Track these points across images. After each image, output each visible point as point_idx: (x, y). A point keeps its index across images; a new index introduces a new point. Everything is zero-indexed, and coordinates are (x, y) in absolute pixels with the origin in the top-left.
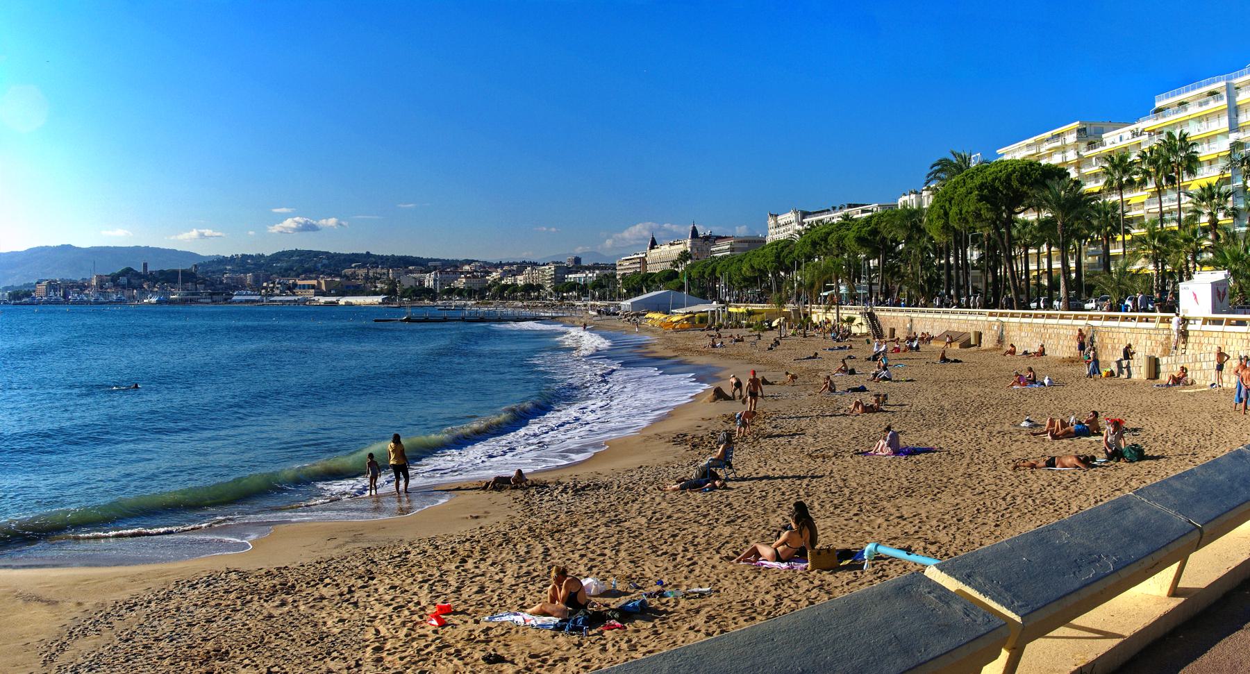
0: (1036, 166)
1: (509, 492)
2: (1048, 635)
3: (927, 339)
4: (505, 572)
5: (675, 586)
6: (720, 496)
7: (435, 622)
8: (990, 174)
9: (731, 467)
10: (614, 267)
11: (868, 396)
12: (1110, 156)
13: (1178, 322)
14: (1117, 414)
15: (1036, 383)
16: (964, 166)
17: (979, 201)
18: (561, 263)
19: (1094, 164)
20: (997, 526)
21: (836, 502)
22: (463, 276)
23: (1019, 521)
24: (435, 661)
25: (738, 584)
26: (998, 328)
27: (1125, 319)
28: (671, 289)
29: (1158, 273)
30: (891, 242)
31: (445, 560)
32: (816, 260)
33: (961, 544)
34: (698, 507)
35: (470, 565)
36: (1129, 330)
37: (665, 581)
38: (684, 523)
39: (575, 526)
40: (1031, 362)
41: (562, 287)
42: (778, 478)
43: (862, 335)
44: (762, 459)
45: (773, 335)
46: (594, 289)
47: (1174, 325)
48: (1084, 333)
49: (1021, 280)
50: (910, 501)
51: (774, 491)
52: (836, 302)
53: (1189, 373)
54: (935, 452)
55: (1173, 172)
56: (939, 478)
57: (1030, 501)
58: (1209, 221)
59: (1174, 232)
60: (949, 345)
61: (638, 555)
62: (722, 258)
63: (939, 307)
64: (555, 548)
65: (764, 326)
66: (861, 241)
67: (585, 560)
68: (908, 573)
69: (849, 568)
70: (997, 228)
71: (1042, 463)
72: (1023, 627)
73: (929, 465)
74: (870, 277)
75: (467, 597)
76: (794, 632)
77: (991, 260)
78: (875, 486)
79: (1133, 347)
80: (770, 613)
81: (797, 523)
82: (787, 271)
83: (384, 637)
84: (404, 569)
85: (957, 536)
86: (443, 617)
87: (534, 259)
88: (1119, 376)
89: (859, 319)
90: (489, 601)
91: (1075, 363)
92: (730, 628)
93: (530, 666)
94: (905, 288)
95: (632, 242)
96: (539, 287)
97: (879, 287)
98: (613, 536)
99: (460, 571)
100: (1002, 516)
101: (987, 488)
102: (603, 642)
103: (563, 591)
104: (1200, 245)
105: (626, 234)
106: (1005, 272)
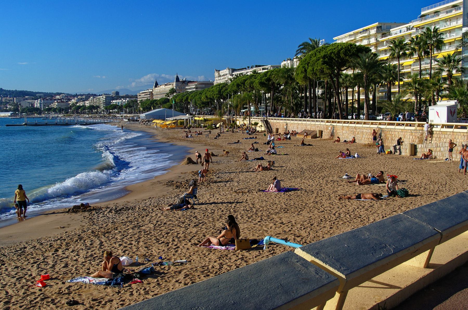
0: (353, 46)
1: (81, 213)
2: (360, 285)
3: (294, 134)
4: (79, 255)
5: (168, 259)
6: (191, 213)
7: (40, 285)
8: (329, 50)
9: (196, 198)
10: (136, 97)
11: (265, 162)
12: (394, 41)
13: (428, 126)
14: (394, 173)
15: (350, 156)
16: (316, 46)
17: (323, 64)
18: (109, 94)
19: (385, 45)
20: (331, 228)
21: (249, 215)
22: (56, 101)
23: (342, 226)
24: (40, 307)
25: (200, 258)
26: (331, 128)
27: (399, 125)
28: (166, 108)
29: (417, 101)
30: (277, 85)
31: (46, 251)
32: (239, 93)
33: (313, 237)
34: (180, 218)
35: (60, 252)
36: (400, 131)
37: (163, 257)
38: (172, 227)
39: (117, 230)
40: (348, 146)
41: (109, 107)
42: (219, 203)
43: (262, 132)
44: (212, 194)
45: (217, 131)
46: (126, 108)
47: (425, 128)
48: (376, 131)
49: (344, 104)
50: (286, 215)
51: (218, 210)
52: (249, 115)
53: (433, 153)
54: (299, 190)
55: (428, 49)
56: (301, 204)
57: (348, 216)
58: (447, 75)
59: (427, 80)
60: (306, 137)
61: (149, 244)
62: (191, 92)
63: (301, 118)
64: (106, 241)
65: (213, 127)
66: (262, 84)
67: (122, 247)
68: (286, 252)
69: (256, 249)
70: (332, 78)
71: (354, 197)
72: (346, 281)
73: (296, 197)
74: (266, 102)
75: (58, 270)
76: (229, 282)
77: (328, 94)
78: (268, 207)
79: (403, 139)
80: (216, 272)
81: (229, 226)
82: (224, 99)
83: (11, 295)
84: (23, 257)
85: (311, 233)
86: (45, 281)
87: (94, 93)
88: (394, 153)
89: (260, 123)
90: (70, 272)
91: (371, 147)
92: (196, 281)
93: (92, 306)
94: (284, 108)
95: (146, 84)
96: (98, 107)
97: (270, 108)
98: (136, 234)
99: (54, 256)
100: (334, 223)
101: (326, 209)
102: (131, 290)
103: (110, 264)
104: (442, 87)
105: (142, 80)
106: (335, 100)
